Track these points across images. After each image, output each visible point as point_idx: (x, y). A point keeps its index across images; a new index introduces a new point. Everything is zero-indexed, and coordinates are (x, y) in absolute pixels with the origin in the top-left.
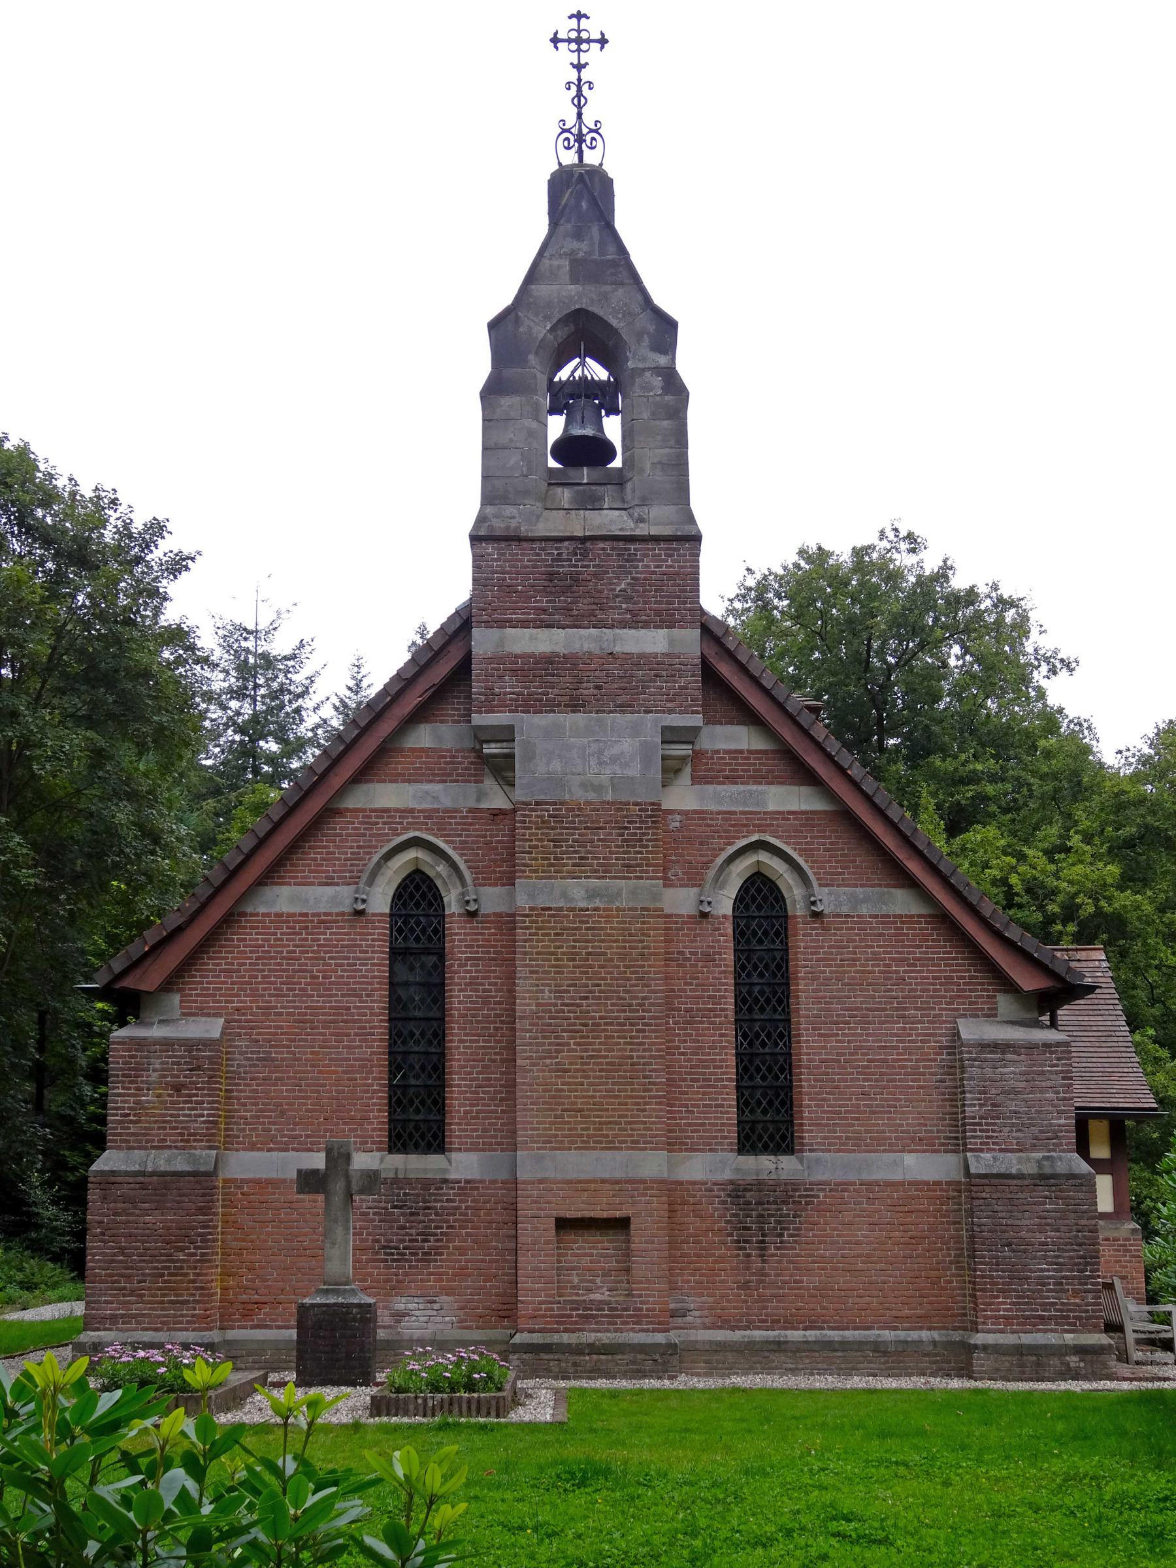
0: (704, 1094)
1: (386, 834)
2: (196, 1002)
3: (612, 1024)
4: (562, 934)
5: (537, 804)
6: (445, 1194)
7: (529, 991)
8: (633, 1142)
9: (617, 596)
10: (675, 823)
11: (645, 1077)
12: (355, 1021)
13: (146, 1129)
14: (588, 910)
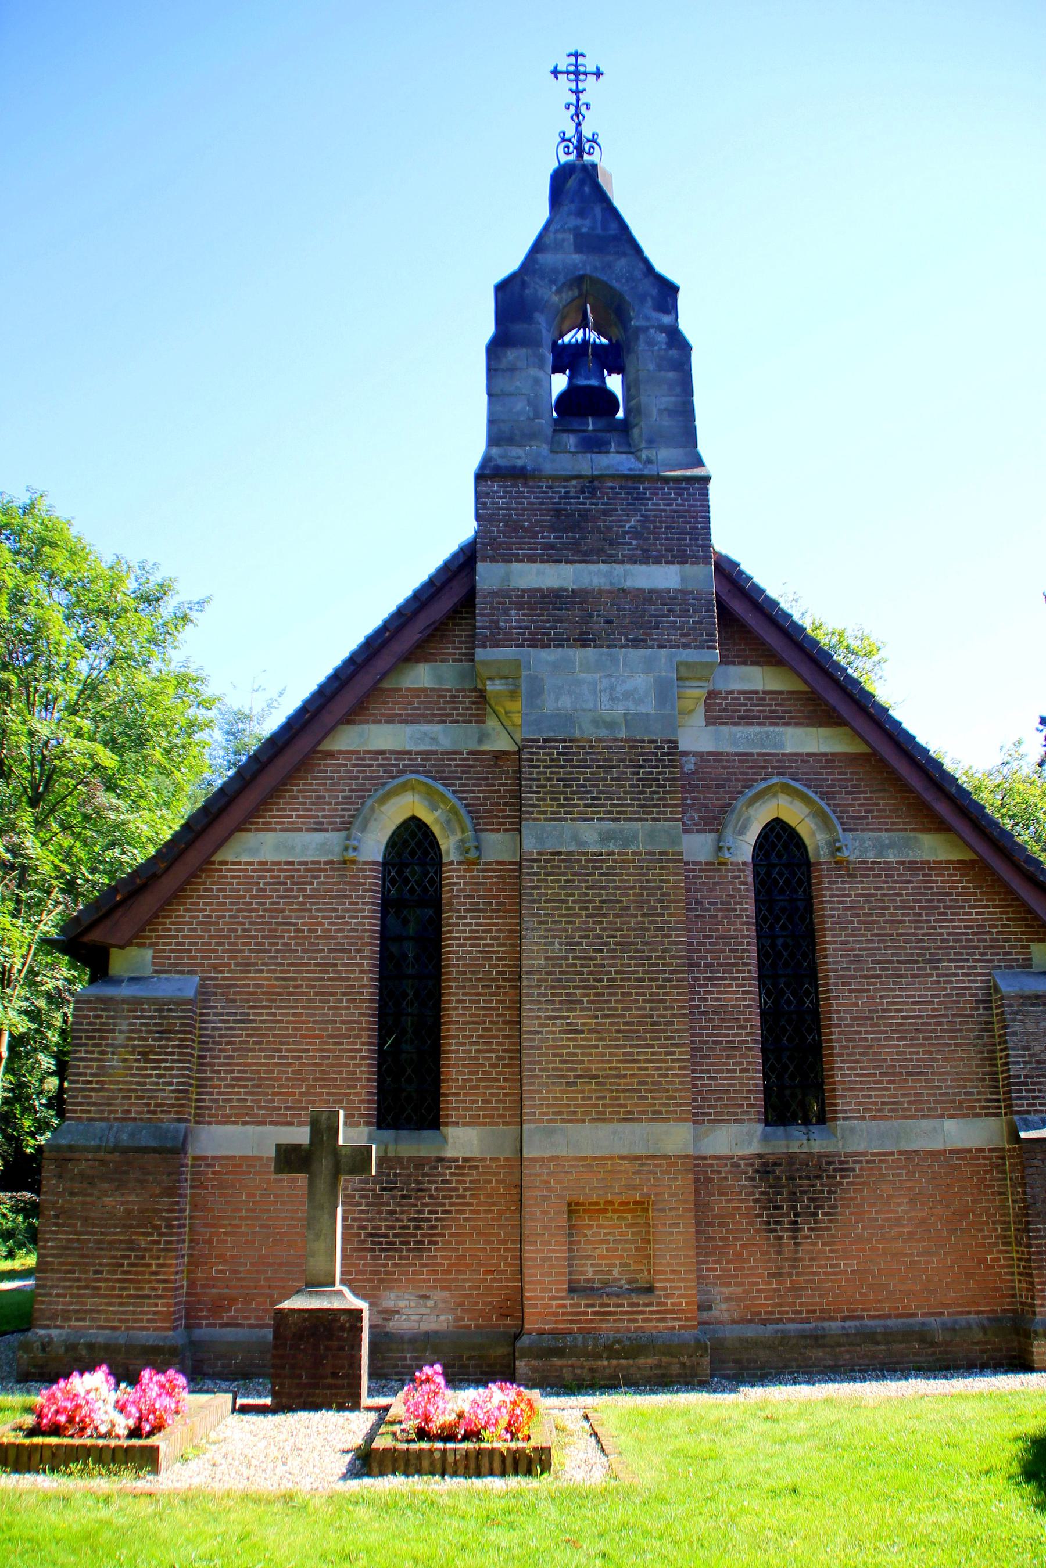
0: (728, 1057)
1: (381, 777)
2: (169, 958)
3: (629, 979)
4: (573, 881)
5: (545, 741)
6: (440, 1174)
7: (537, 944)
8: (654, 1112)
9: (627, 533)
10: (690, 765)
11: (667, 1038)
12: (342, 979)
13: (109, 1098)
14: (601, 854)
